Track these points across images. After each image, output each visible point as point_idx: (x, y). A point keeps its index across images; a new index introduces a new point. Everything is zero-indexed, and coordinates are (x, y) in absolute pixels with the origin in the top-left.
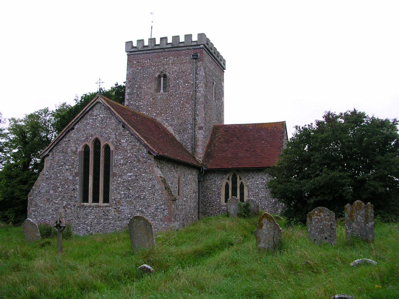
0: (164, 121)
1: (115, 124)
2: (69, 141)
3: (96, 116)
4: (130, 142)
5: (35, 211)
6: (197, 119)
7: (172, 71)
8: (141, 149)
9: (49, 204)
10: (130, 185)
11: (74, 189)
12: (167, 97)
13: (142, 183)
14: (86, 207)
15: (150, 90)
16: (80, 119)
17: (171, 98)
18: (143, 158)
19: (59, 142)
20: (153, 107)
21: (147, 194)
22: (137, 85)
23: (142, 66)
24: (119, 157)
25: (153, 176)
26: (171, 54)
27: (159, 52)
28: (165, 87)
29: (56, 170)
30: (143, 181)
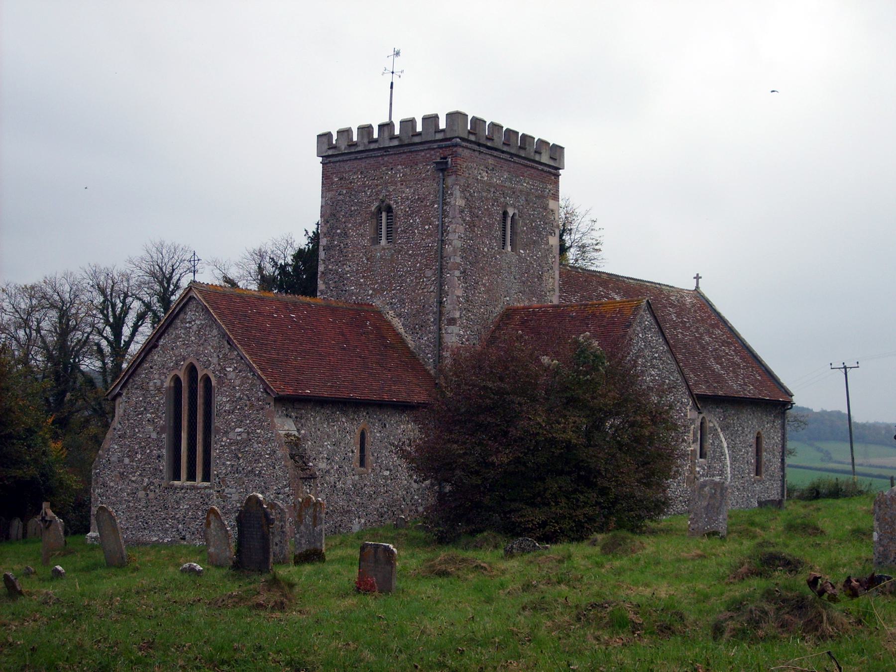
0: (388, 305)
1: (219, 338)
2: (151, 368)
3: (190, 322)
4: (239, 372)
5: (103, 496)
6: (444, 302)
8: (255, 385)
9: (123, 482)
10: (239, 450)
11: (159, 456)
12: (392, 255)
13: (257, 446)
14: (176, 488)
15: (362, 239)
16: (167, 328)
17: (400, 256)
18: (258, 400)
19: (135, 370)
20: (368, 277)
21: (264, 466)
22: (339, 229)
23: (349, 188)
24: (224, 399)
25: (272, 433)
26: (400, 159)
27: (379, 156)
29: (132, 421)
30: (258, 443)
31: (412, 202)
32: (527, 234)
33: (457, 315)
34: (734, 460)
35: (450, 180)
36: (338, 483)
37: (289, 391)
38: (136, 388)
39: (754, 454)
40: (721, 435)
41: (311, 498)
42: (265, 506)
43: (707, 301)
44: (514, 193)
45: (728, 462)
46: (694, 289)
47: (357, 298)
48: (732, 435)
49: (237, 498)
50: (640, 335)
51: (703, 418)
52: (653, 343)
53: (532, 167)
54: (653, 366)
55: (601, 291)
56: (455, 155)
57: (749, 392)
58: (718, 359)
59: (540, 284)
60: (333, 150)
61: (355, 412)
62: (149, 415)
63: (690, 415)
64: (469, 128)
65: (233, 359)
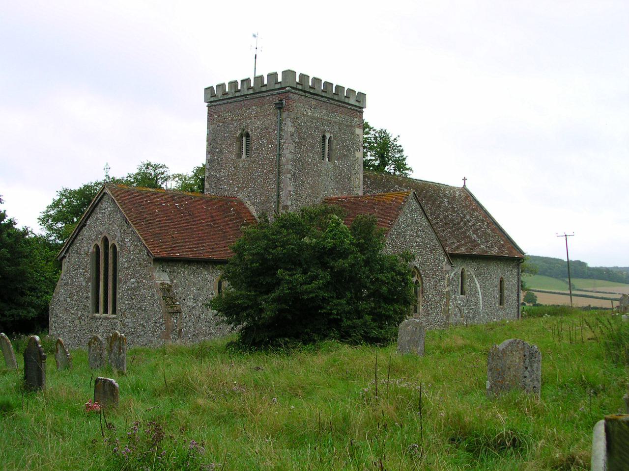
3: (104, 209)
7: (255, 126)
8: (142, 251)
11: (87, 297)
16: (91, 213)
18: (144, 260)
19: (73, 241)
25: (152, 283)
26: (254, 102)
27: (241, 101)
28: (247, 151)
29: (72, 274)
31: (261, 130)
32: (339, 150)
33: (289, 203)
34: (484, 295)
35: (284, 115)
36: (201, 315)
37: (164, 254)
38: (74, 253)
39: (498, 292)
40: (476, 280)
41: (117, 334)
42: (40, 346)
43: (471, 194)
44: (330, 123)
45: (481, 297)
46: (462, 186)
47: (228, 193)
48: (483, 280)
49: (132, 326)
50: (409, 215)
51: (463, 269)
52: (418, 221)
53: (343, 107)
54: (418, 236)
55: (396, 188)
56: (288, 98)
57: (495, 252)
58: (475, 231)
59: (349, 183)
60: (214, 98)
61: (214, 268)
62: (81, 270)
63: (445, 268)
64: (322, 89)
65: (129, 233)
